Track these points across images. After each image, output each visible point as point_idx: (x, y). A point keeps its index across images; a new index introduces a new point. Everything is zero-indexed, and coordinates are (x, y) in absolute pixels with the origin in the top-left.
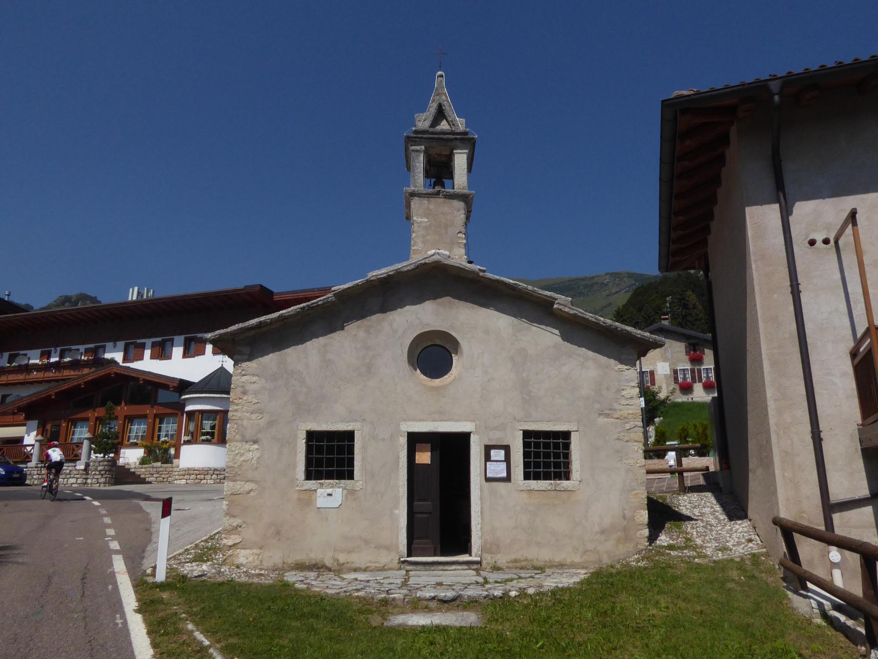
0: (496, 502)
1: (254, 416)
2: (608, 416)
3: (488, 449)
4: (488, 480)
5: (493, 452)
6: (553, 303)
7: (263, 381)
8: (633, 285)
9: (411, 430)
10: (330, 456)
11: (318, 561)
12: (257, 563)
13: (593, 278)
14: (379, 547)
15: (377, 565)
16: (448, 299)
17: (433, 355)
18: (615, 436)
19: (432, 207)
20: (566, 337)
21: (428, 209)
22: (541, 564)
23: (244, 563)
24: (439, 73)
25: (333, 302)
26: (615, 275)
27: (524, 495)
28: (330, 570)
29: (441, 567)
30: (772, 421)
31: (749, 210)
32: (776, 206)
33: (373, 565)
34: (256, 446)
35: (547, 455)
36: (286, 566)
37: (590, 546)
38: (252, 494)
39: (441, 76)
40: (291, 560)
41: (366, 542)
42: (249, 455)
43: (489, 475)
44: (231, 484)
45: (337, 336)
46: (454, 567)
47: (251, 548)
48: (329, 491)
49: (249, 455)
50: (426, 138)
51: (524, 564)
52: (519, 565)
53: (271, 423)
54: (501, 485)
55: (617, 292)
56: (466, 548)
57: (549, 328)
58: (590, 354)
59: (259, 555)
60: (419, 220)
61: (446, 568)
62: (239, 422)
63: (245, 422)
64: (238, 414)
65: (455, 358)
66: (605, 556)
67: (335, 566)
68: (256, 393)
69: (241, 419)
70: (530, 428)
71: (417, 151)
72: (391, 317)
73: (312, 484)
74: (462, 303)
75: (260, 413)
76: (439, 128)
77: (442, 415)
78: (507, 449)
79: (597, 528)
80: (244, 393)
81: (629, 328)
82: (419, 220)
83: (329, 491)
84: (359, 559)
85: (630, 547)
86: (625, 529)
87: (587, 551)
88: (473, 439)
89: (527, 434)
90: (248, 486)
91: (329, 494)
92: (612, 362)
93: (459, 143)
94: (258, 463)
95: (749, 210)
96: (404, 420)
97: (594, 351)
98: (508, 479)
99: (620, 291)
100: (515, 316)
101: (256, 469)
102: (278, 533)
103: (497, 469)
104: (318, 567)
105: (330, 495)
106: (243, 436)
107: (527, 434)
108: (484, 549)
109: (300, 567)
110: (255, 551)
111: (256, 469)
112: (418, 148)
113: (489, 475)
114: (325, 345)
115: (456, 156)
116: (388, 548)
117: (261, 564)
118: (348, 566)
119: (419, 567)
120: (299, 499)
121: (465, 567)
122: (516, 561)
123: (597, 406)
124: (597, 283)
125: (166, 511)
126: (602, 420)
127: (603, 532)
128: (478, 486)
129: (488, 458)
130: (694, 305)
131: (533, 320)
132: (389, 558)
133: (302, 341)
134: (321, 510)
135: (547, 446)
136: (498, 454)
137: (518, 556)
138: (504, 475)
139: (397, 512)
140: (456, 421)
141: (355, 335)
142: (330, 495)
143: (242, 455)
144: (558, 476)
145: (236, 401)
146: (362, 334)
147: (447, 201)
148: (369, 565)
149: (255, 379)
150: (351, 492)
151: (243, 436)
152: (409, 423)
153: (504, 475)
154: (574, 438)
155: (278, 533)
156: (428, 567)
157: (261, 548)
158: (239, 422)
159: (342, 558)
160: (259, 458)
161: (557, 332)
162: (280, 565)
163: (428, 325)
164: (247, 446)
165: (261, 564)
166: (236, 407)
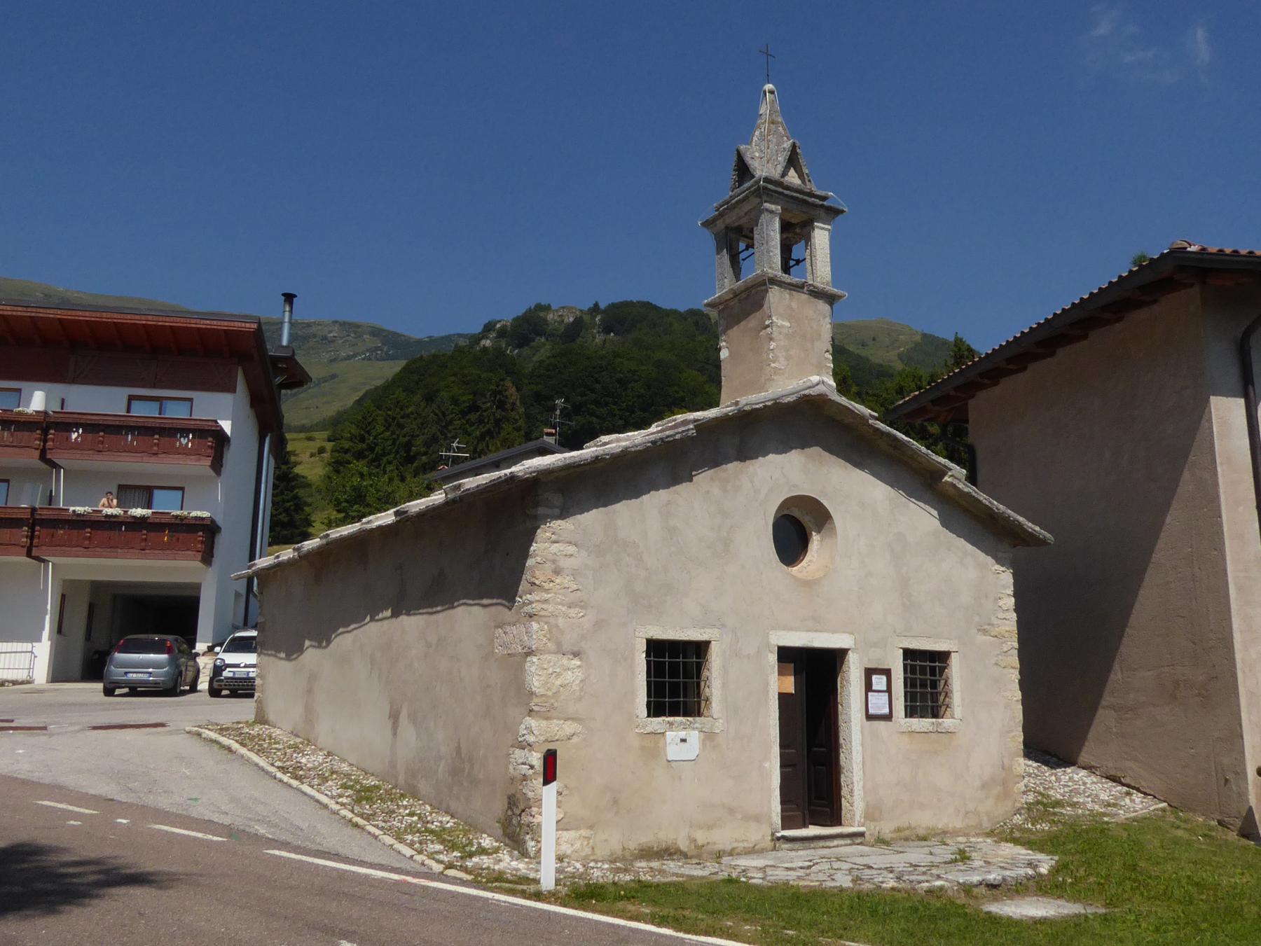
0: (873, 746)
1: (573, 612)
2: (985, 632)
3: (869, 673)
4: (870, 717)
5: (875, 678)
6: (945, 474)
7: (584, 554)
8: (377, 348)
9: (781, 644)
10: (676, 678)
11: (669, 843)
12: (588, 851)
13: (309, 325)
14: (747, 818)
15: (746, 845)
16: (816, 450)
17: (795, 530)
18: (994, 660)
19: (794, 305)
20: (945, 522)
21: (790, 307)
22: (922, 832)
23: (569, 852)
24: (769, 87)
25: (691, 438)
26: (348, 327)
27: (906, 738)
28: (685, 856)
29: (821, 843)
30: (1238, 656)
31: (1214, 400)
32: (1242, 401)
33: (741, 845)
34: (577, 662)
35: (925, 680)
36: (627, 854)
37: (971, 807)
38: (575, 740)
39: (772, 92)
40: (632, 845)
41: (731, 811)
42: (569, 676)
43: (871, 711)
44: (544, 723)
45: (683, 488)
46: (836, 842)
47: (577, 828)
48: (683, 734)
49: (569, 676)
50: (787, 196)
51: (907, 833)
52: (902, 835)
53: (599, 625)
54: (882, 724)
55: (348, 358)
56: (834, 817)
57: (921, 504)
58: (969, 547)
59: (588, 838)
60: (780, 322)
61: (828, 843)
62: (552, 620)
63: (561, 621)
64: (550, 608)
65: (815, 540)
66: (985, 818)
67: (692, 852)
68: (575, 574)
69: (553, 615)
70: (911, 647)
71: (772, 212)
72: (751, 469)
73: (658, 723)
74: (833, 458)
75: (582, 607)
76: (786, 178)
77: (818, 624)
78: (887, 673)
79: (978, 783)
80: (557, 572)
81: (1021, 519)
82: (780, 322)
83: (683, 734)
84: (722, 838)
85: (1007, 806)
86: (1004, 783)
87: (967, 813)
88: (852, 658)
89: (909, 654)
90: (569, 728)
91: (681, 739)
92: (990, 560)
93: (822, 213)
94: (581, 690)
95: (1214, 400)
96: (773, 628)
97: (973, 544)
98: (888, 717)
99: (355, 355)
100: (892, 486)
101: (580, 699)
102: (616, 801)
103: (879, 704)
104: (668, 852)
105: (683, 740)
106: (559, 644)
107: (909, 654)
108: (869, 816)
109: (647, 853)
110: (584, 832)
111: (580, 699)
112: (773, 207)
113: (871, 711)
114: (669, 503)
115: (817, 231)
116: (757, 819)
117: (593, 854)
118: (709, 847)
119: (797, 845)
120: (642, 748)
121: (849, 841)
122: (899, 830)
123: (977, 619)
124: (315, 336)
125: (549, 775)
126: (981, 638)
127: (983, 787)
128: (859, 728)
129: (868, 687)
130: (514, 404)
131: (911, 493)
132: (759, 834)
133: (636, 493)
134: (673, 764)
135: (923, 669)
136: (879, 682)
137: (903, 822)
138: (886, 711)
139: (767, 765)
140: (834, 632)
141: (708, 492)
142: (683, 740)
143: (559, 675)
144: (935, 716)
145: (546, 586)
146: (716, 491)
147: (813, 299)
148: (735, 845)
149: (571, 549)
150: (709, 737)
151: (559, 644)
152: (780, 633)
153: (886, 711)
154: (954, 660)
155: (616, 801)
156: (807, 845)
157: (591, 827)
158: (552, 620)
159: (701, 836)
160: (582, 681)
161: (935, 513)
162: (619, 853)
163: (795, 486)
164: (565, 661)
165: (593, 854)
166: (546, 596)
